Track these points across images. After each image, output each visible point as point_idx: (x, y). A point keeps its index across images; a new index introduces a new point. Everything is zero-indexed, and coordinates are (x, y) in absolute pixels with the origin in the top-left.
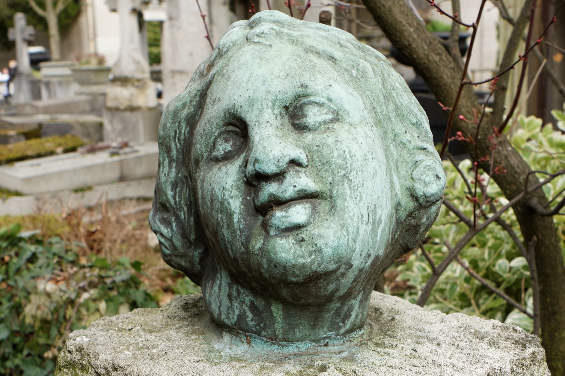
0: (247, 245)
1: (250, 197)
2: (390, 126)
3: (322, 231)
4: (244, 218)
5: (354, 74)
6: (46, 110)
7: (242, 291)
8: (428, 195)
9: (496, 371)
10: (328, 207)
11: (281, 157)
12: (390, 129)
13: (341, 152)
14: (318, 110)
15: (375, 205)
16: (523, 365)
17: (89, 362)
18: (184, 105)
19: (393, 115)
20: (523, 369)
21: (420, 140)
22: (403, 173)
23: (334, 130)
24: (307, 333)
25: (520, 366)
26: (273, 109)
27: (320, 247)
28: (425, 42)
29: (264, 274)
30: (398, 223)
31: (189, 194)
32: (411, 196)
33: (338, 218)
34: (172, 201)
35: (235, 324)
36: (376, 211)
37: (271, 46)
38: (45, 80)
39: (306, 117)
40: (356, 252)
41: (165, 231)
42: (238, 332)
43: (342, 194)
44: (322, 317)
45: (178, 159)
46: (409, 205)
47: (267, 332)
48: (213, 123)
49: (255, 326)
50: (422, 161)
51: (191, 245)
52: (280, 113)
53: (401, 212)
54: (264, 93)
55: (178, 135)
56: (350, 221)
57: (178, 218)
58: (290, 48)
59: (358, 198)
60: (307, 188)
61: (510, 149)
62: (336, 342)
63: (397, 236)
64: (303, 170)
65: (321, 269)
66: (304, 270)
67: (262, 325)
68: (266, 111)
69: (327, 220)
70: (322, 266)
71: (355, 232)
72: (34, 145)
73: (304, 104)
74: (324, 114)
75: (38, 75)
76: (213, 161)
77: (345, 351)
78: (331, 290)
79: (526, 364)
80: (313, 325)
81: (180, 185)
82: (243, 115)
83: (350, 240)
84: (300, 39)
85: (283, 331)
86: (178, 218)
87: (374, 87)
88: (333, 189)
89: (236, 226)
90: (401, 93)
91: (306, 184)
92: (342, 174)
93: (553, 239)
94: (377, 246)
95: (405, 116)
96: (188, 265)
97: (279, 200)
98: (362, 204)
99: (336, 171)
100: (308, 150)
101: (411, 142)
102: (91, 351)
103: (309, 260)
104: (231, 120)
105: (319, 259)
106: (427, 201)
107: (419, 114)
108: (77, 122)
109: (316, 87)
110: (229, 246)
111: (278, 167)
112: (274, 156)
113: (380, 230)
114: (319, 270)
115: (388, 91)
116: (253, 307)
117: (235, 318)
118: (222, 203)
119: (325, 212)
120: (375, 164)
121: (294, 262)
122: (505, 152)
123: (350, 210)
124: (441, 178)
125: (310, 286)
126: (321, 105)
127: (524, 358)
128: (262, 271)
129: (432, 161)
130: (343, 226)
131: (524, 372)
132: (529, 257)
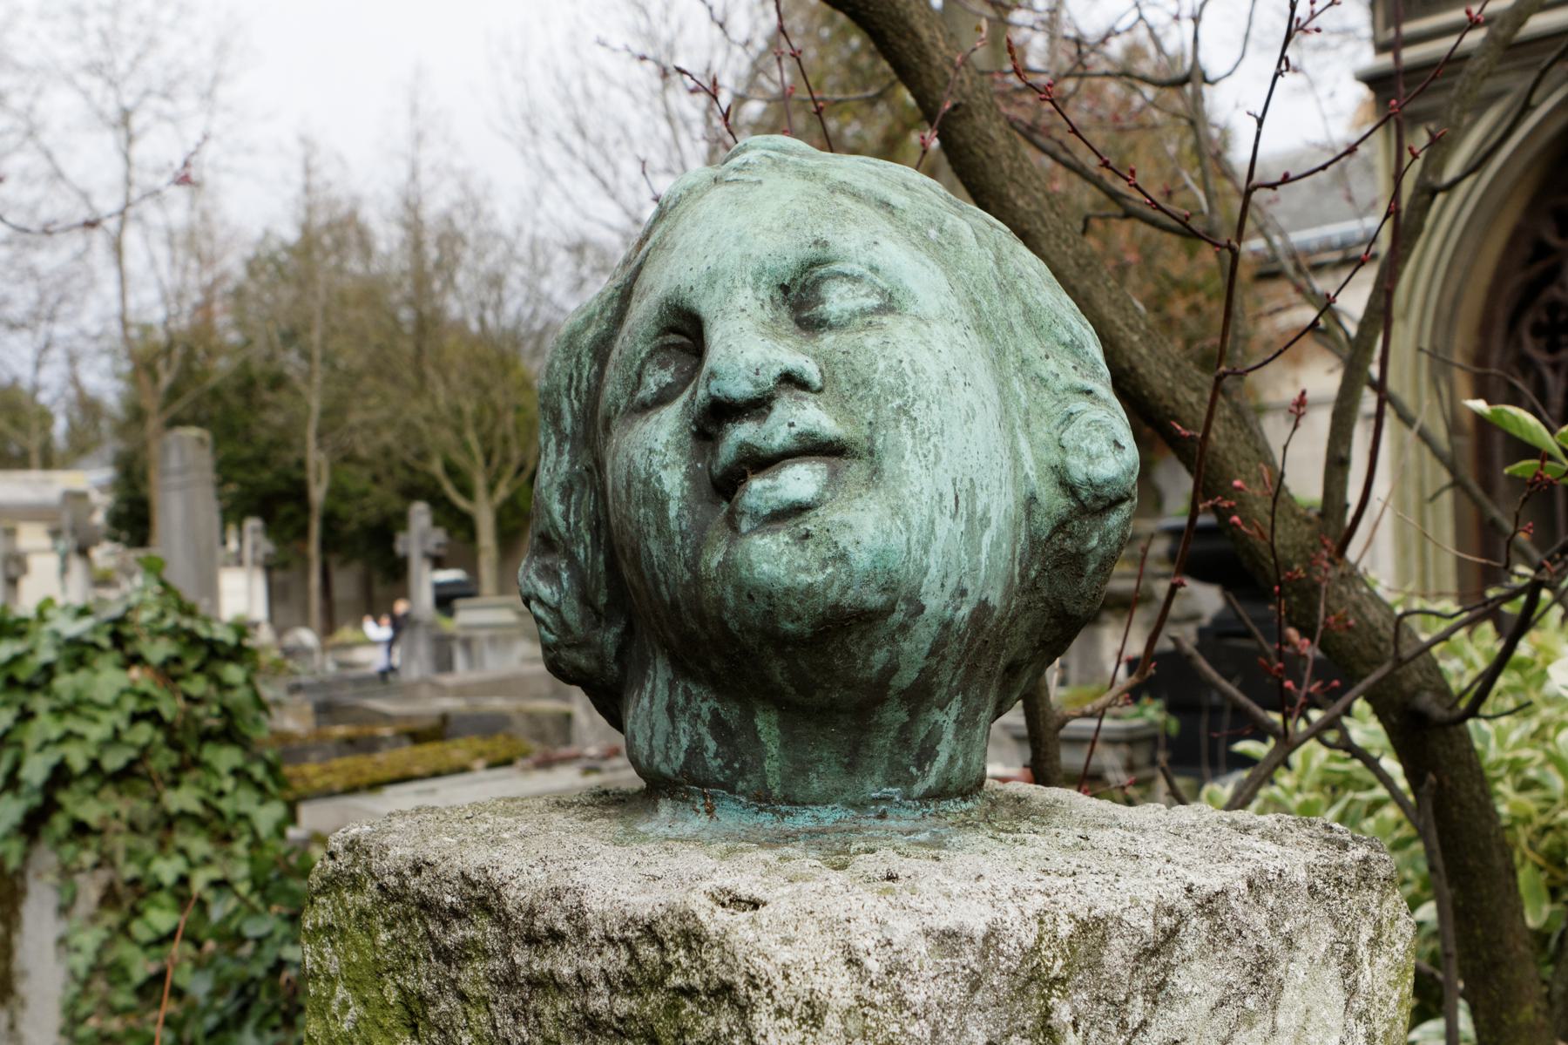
0: (696, 564)
1: (703, 463)
3: (850, 517)
4: (689, 507)
6: (461, 691)
7: (694, 692)
8: (1098, 481)
9: (1270, 877)
10: (865, 473)
11: (763, 365)
12: (1012, 348)
13: (894, 362)
15: (971, 480)
16: (1339, 879)
17: (367, 867)
18: (589, 321)
19: (1018, 322)
20: (1341, 891)
23: (881, 326)
24: (837, 785)
25: (1332, 882)
26: (756, 289)
27: (845, 548)
28: (1166, 363)
29: (730, 625)
30: (1033, 541)
31: (596, 506)
32: (1061, 484)
34: (561, 524)
35: (682, 772)
36: (974, 494)
37: (760, 182)
38: (461, 634)
39: (823, 303)
40: (929, 576)
41: (545, 590)
42: (688, 792)
44: (868, 746)
45: (574, 433)
47: (749, 782)
48: (637, 333)
49: (722, 769)
51: (599, 620)
52: (772, 298)
53: (1038, 518)
54: (738, 259)
55: (574, 383)
56: (912, 501)
57: (572, 558)
58: (797, 185)
59: (931, 458)
61: (1365, 590)
62: (903, 813)
63: (1033, 574)
64: (812, 396)
65: (849, 598)
66: (810, 601)
67: (737, 765)
69: (860, 496)
70: (851, 592)
72: (430, 753)
73: (822, 278)
75: (448, 625)
76: (636, 412)
77: (924, 831)
78: (879, 666)
79: (1346, 878)
80: (850, 764)
81: (577, 488)
82: (695, 304)
83: (913, 542)
85: (783, 778)
86: (572, 558)
88: (876, 436)
89: (674, 525)
90: (1037, 285)
92: (894, 405)
93: (1477, 788)
94: (982, 574)
95: (1046, 327)
96: (594, 664)
97: (758, 456)
98: (939, 470)
99: (882, 400)
100: (826, 363)
102: (374, 845)
103: (821, 577)
104: (672, 321)
105: (843, 577)
106: (1097, 498)
107: (1076, 326)
108: (520, 711)
109: (846, 244)
110: (661, 576)
111: (757, 385)
112: (747, 361)
113: (986, 540)
114: (845, 602)
115: (1009, 278)
116: (718, 726)
117: (682, 756)
118: (646, 483)
120: (967, 396)
121: (787, 581)
122: (1354, 597)
125: (829, 649)
126: (856, 279)
128: (726, 615)
130: (896, 511)
131: (1344, 897)
132: (1421, 821)
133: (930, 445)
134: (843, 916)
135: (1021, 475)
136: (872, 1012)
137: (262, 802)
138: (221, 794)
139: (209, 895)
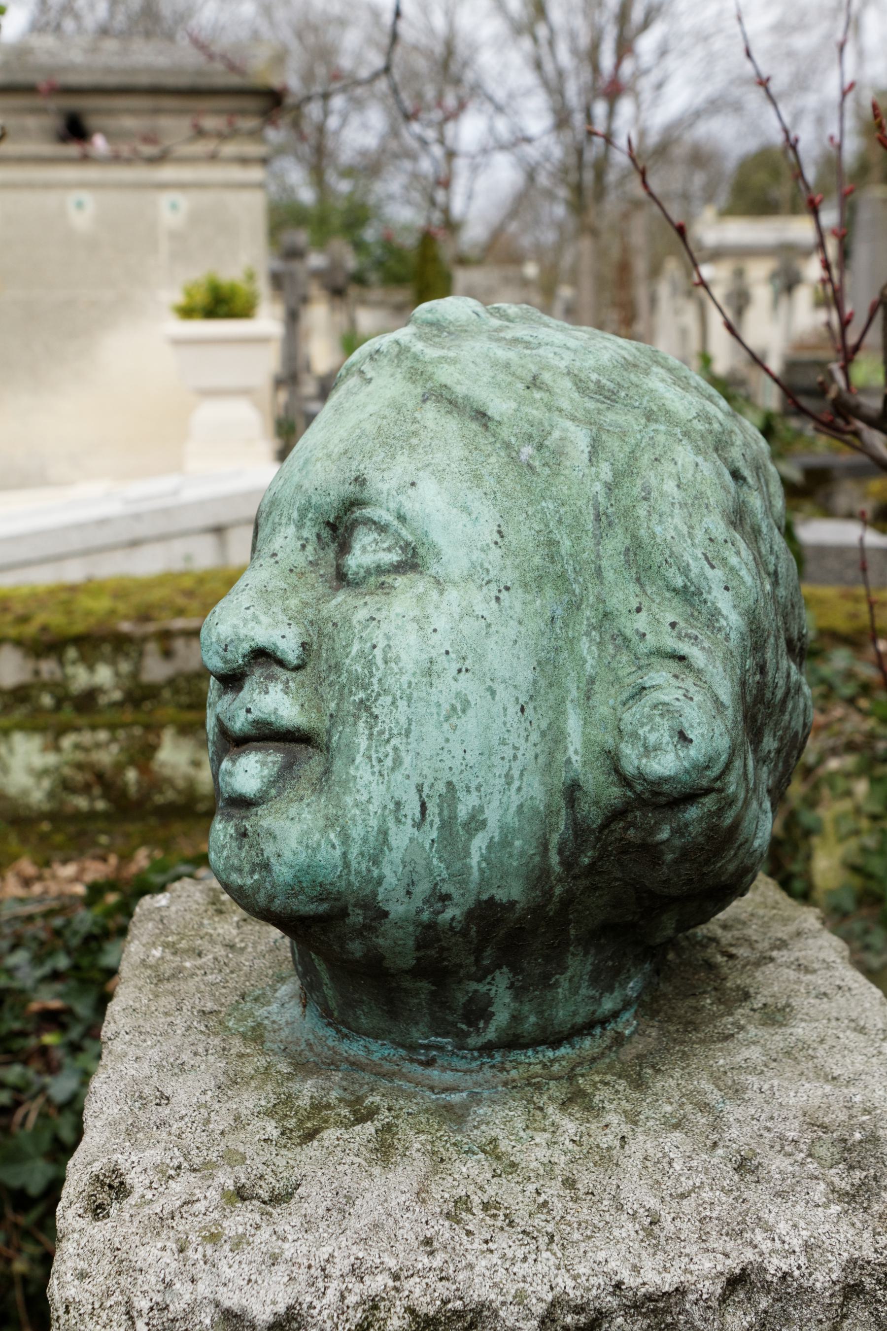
5: (523, 457)
9: (769, 1278)
11: (232, 641)
12: (592, 599)
14: (375, 540)
15: (450, 784)
21: (674, 634)
22: (604, 710)
26: (300, 526)
33: (328, 800)
43: (347, 745)
46: (607, 792)
52: (318, 536)
59: (389, 762)
60: (273, 719)
62: (457, 1063)
64: (284, 674)
68: (283, 530)
71: (371, 839)
74: (384, 550)
77: (462, 1091)
87: (574, 491)
88: (334, 731)
91: (272, 708)
92: (357, 699)
95: (655, 568)
98: (398, 776)
99: (346, 690)
101: (644, 635)
103: (249, 882)
106: (656, 794)
109: (380, 485)
111: (226, 662)
123: (358, 787)
124: (691, 741)
126: (382, 528)
129: (679, 694)
130: (331, 822)
133: (389, 748)
134: (139, 1265)
135: (560, 758)
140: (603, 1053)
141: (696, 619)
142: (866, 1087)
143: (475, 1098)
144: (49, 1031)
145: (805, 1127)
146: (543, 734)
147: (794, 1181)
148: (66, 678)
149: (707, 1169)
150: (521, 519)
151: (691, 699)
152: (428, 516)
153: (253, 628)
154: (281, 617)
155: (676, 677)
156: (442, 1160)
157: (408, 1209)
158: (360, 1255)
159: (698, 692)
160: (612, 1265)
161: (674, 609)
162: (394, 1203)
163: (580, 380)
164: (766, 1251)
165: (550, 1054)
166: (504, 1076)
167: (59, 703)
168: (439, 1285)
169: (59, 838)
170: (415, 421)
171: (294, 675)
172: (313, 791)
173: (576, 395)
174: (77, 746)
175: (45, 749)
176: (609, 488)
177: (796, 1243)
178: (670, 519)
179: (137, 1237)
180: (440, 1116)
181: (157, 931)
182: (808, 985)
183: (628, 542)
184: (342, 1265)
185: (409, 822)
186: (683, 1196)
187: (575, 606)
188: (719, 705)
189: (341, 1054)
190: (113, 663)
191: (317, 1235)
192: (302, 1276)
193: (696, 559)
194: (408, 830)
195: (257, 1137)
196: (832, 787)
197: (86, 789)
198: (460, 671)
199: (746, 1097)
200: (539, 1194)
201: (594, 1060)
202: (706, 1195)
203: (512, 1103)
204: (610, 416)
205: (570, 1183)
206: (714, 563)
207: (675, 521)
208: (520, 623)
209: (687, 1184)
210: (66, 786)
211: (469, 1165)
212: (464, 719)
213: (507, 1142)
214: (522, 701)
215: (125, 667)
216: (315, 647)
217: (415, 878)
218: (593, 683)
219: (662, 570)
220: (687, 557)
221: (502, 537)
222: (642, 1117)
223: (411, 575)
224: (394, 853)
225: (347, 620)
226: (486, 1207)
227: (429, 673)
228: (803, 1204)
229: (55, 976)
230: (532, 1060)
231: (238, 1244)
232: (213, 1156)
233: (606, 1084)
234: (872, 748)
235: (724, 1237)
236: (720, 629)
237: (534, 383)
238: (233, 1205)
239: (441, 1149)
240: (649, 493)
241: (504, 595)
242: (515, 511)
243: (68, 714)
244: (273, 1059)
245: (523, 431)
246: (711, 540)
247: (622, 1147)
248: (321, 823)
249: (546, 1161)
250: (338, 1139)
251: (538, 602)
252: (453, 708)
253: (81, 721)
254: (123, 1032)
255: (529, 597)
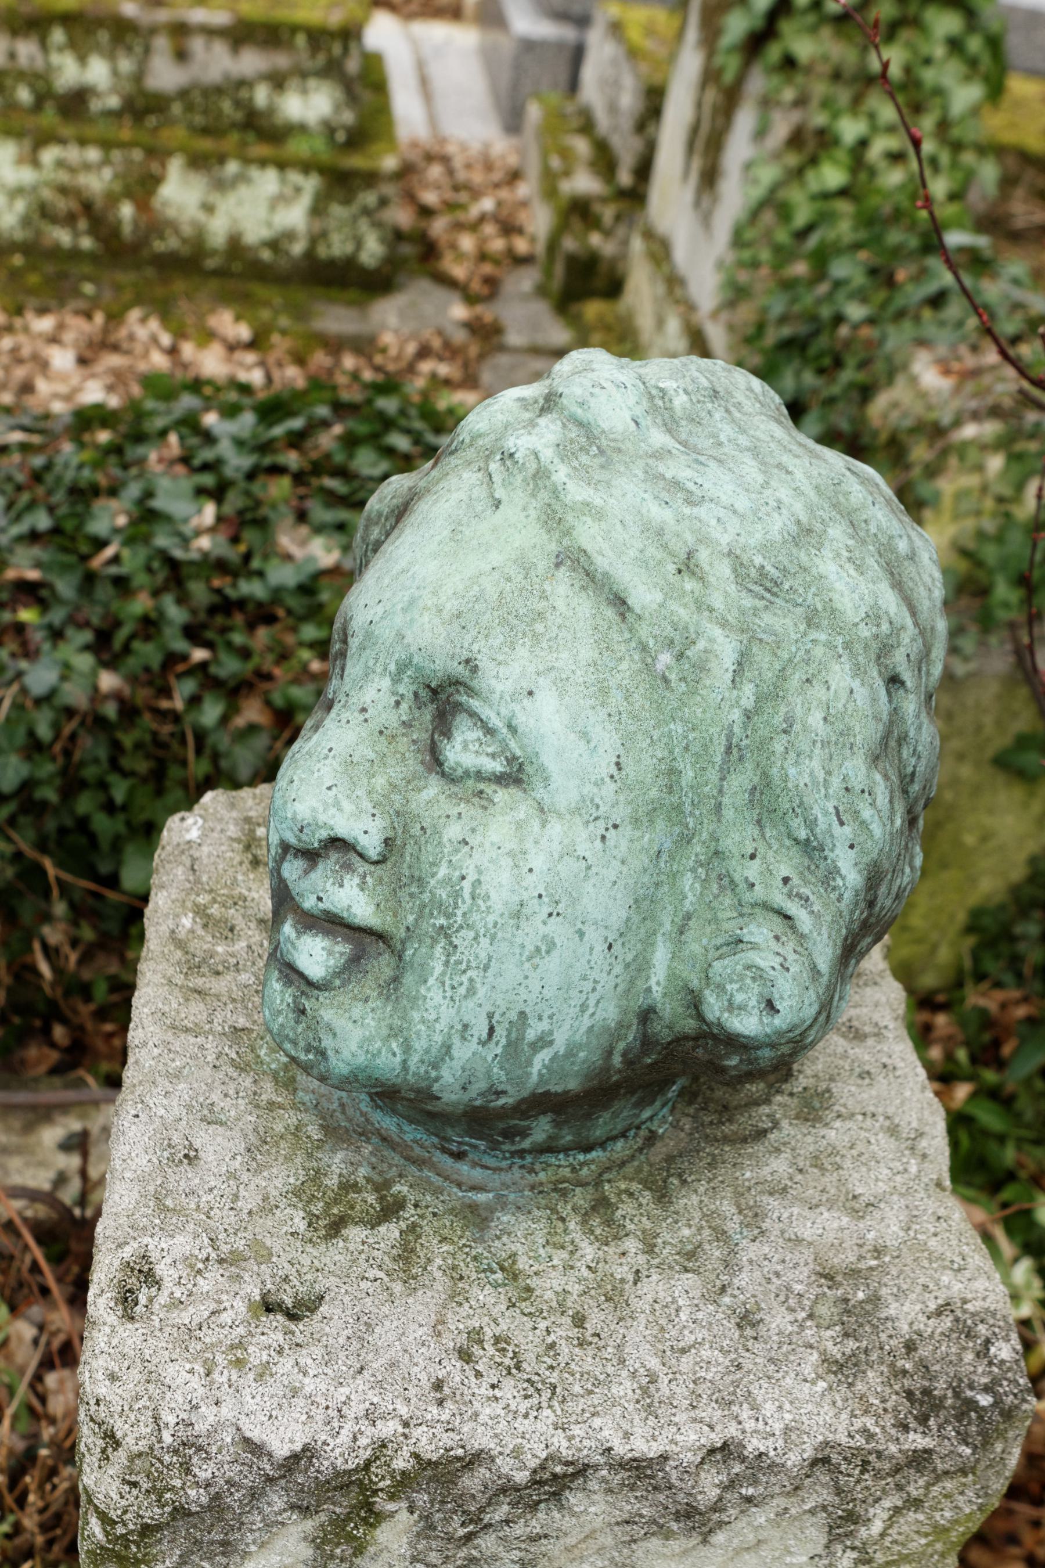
2: (708, 828)
5: (660, 666)
9: (746, 1453)
10: (388, 972)
11: (309, 825)
12: (705, 835)
21: (785, 890)
22: (696, 948)
26: (396, 680)
33: (394, 1009)
46: (683, 1022)
50: (754, 946)
52: (416, 694)
59: (462, 990)
60: (345, 915)
64: (362, 867)
68: (376, 680)
73: (458, 707)
77: (489, 1191)
84: (570, 518)
87: (708, 715)
88: (408, 945)
98: (470, 1004)
99: (427, 910)
101: (753, 885)
109: (493, 682)
119: (377, 979)
124: (778, 1011)
127: (879, 1454)
130: (394, 1032)
133: (464, 979)
134: (167, 1381)
135: (641, 985)
136: (158, 1465)
137: (967, 79)
138: (928, 61)
139: (882, 164)
140: (633, 1156)
141: (812, 873)
142: (882, 1219)
143: (501, 1203)
144: (26, 606)
145: (813, 1278)
146: (627, 966)
147: (790, 1347)
148: (49, 67)
149: (711, 1324)
150: (644, 745)
151: (788, 970)
152: (542, 736)
153: (334, 816)
154: (366, 805)
155: (777, 938)
156: (461, 1278)
157: (423, 1345)
158: (375, 1400)
159: (796, 961)
160: (606, 1433)
161: (791, 859)
162: (411, 1338)
163: (742, 564)
164: (749, 1430)
165: (581, 1157)
166: (531, 1178)
167: (38, 106)
168: (445, 1435)
169: (33, 279)
170: (543, 597)
171: (372, 868)
172: (380, 994)
173: (732, 588)
174: (60, 164)
175: (20, 161)
176: (748, 715)
177: (778, 1427)
178: (807, 761)
179: (167, 1353)
180: (465, 1217)
181: (188, 885)
182: (853, 1061)
183: (756, 780)
184: (357, 1409)
185: (475, 1040)
186: (684, 1351)
187: (686, 839)
188: (815, 971)
189: (373, 1124)
190: (111, 57)
191: (336, 1367)
192: (319, 1415)
193: (826, 813)
194: (473, 1046)
195: (285, 1229)
196: (962, 458)
197: (69, 220)
198: (550, 915)
199: (764, 1226)
200: (548, 1332)
201: (623, 1164)
202: (706, 1353)
203: (537, 1213)
204: (767, 618)
205: (579, 1321)
206: (844, 818)
207: (814, 763)
208: (623, 862)
209: (689, 1339)
210: (45, 212)
211: (486, 1292)
212: (547, 959)
213: (525, 1258)
214: (610, 940)
215: (126, 65)
216: (398, 842)
217: (473, 1079)
218: (689, 919)
219: (787, 818)
220: (816, 811)
221: (620, 769)
222: (660, 1241)
223: (513, 790)
224: (454, 1062)
225: (437, 832)
226: (497, 1340)
227: (517, 915)
228: (793, 1375)
229: (34, 537)
230: (562, 1163)
231: (261, 1375)
232: (240, 1245)
233: (631, 1195)
234: (1020, 418)
235: (713, 1404)
236: (834, 889)
237: (688, 566)
238: (258, 1320)
239: (462, 1264)
240: (791, 726)
241: (611, 834)
242: (640, 736)
243: (49, 117)
244: (305, 1117)
245: (664, 634)
246: (847, 789)
247: (635, 1284)
248: (385, 1031)
249: (559, 1289)
250: (363, 1243)
251: (647, 837)
252: (538, 950)
253: (67, 131)
254: (151, 1043)
255: (638, 833)
